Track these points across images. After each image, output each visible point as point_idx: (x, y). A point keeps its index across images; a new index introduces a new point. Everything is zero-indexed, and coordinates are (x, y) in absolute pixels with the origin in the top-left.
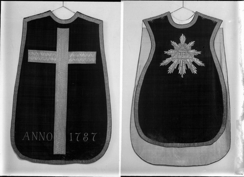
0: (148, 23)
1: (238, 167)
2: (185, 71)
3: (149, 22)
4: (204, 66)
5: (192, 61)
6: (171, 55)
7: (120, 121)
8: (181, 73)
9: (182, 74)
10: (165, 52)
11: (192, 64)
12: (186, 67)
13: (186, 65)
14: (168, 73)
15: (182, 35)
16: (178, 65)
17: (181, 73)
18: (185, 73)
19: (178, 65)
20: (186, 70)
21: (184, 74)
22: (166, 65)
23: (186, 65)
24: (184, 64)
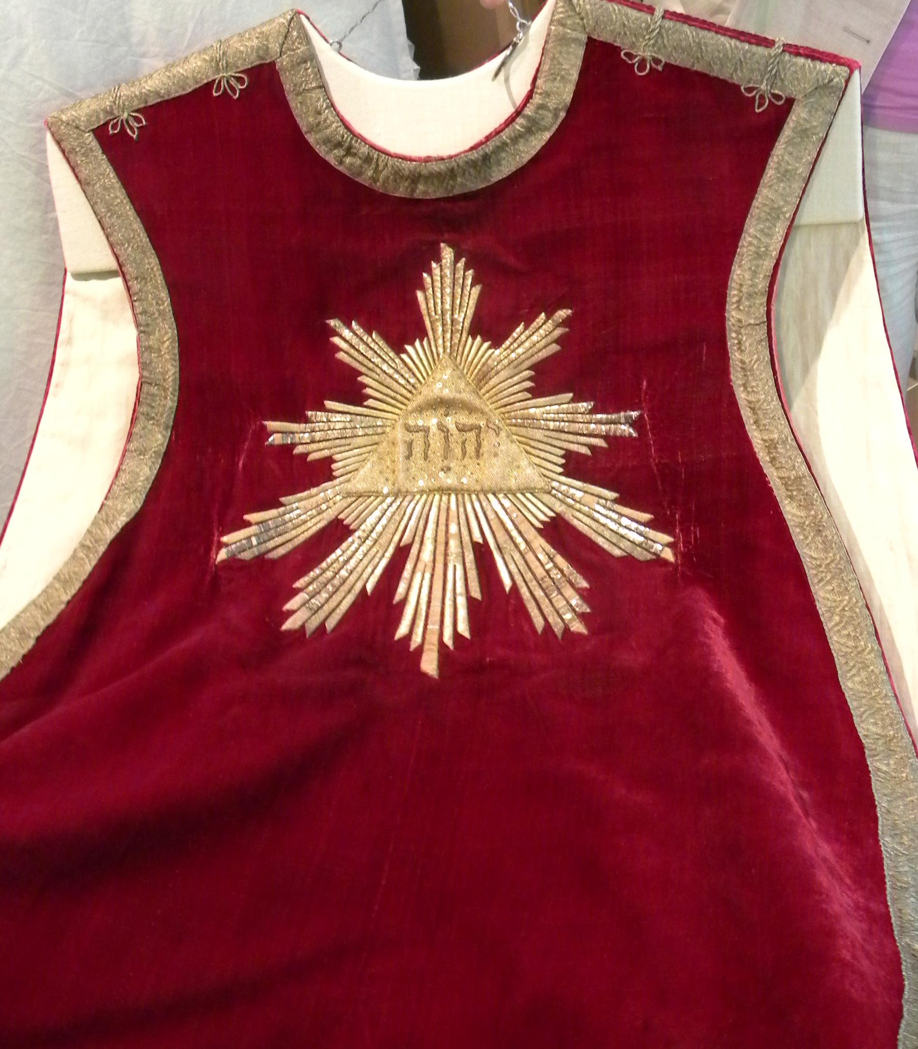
0: (95, 144)
1: (352, 150)
2: (462, 613)
3: (100, 133)
4: (668, 555)
5: (541, 513)
6: (329, 460)
7: (337, 404)
8: (419, 630)
9: (433, 639)
10: (271, 425)
11: (540, 543)
12: (473, 574)
13: (483, 554)
14: (289, 624)
15: (438, 260)
16: (401, 554)
17: (419, 630)
18: (457, 636)
19: (401, 554)
20: (470, 600)
21: (448, 639)
22: (274, 555)
23: (483, 554)
24: (453, 544)
